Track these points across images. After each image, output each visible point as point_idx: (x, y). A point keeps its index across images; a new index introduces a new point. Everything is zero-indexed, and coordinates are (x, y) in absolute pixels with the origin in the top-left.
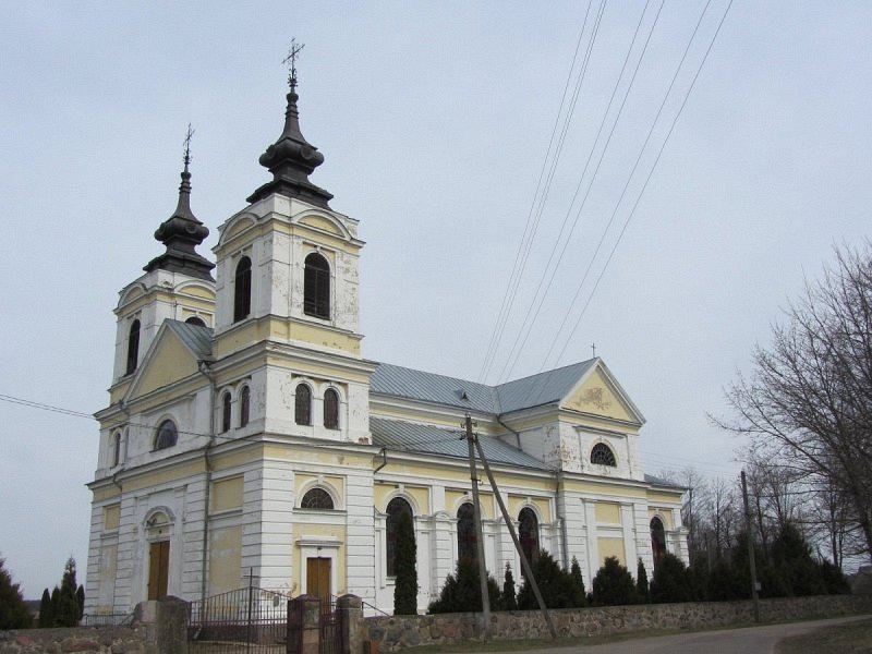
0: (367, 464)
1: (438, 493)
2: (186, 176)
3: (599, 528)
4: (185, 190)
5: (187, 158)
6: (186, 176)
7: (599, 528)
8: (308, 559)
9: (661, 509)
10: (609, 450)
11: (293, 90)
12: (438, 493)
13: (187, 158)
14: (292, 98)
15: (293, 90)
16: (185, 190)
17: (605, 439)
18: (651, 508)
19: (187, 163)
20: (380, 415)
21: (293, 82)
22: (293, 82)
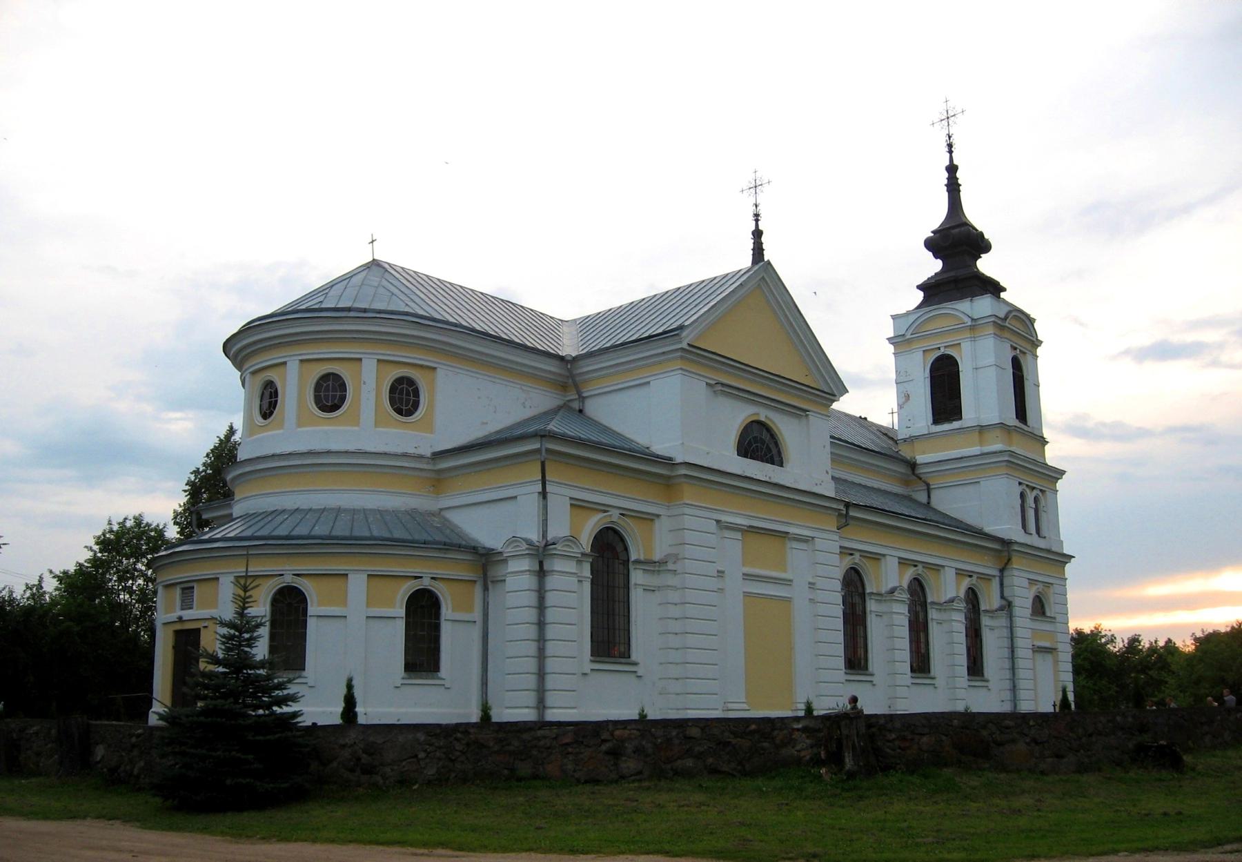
0: (831, 523)
1: (949, 575)
2: (952, 169)
3: (747, 577)
4: (953, 187)
5: (950, 146)
6: (952, 169)
7: (747, 577)
8: (376, 426)
9: (926, 565)
10: (773, 436)
11: (757, 225)
12: (949, 575)
13: (950, 146)
14: (757, 234)
15: (757, 225)
16: (953, 187)
17: (763, 415)
18: (1032, 582)
19: (951, 152)
20: (832, 450)
21: (757, 217)
22: (757, 217)
